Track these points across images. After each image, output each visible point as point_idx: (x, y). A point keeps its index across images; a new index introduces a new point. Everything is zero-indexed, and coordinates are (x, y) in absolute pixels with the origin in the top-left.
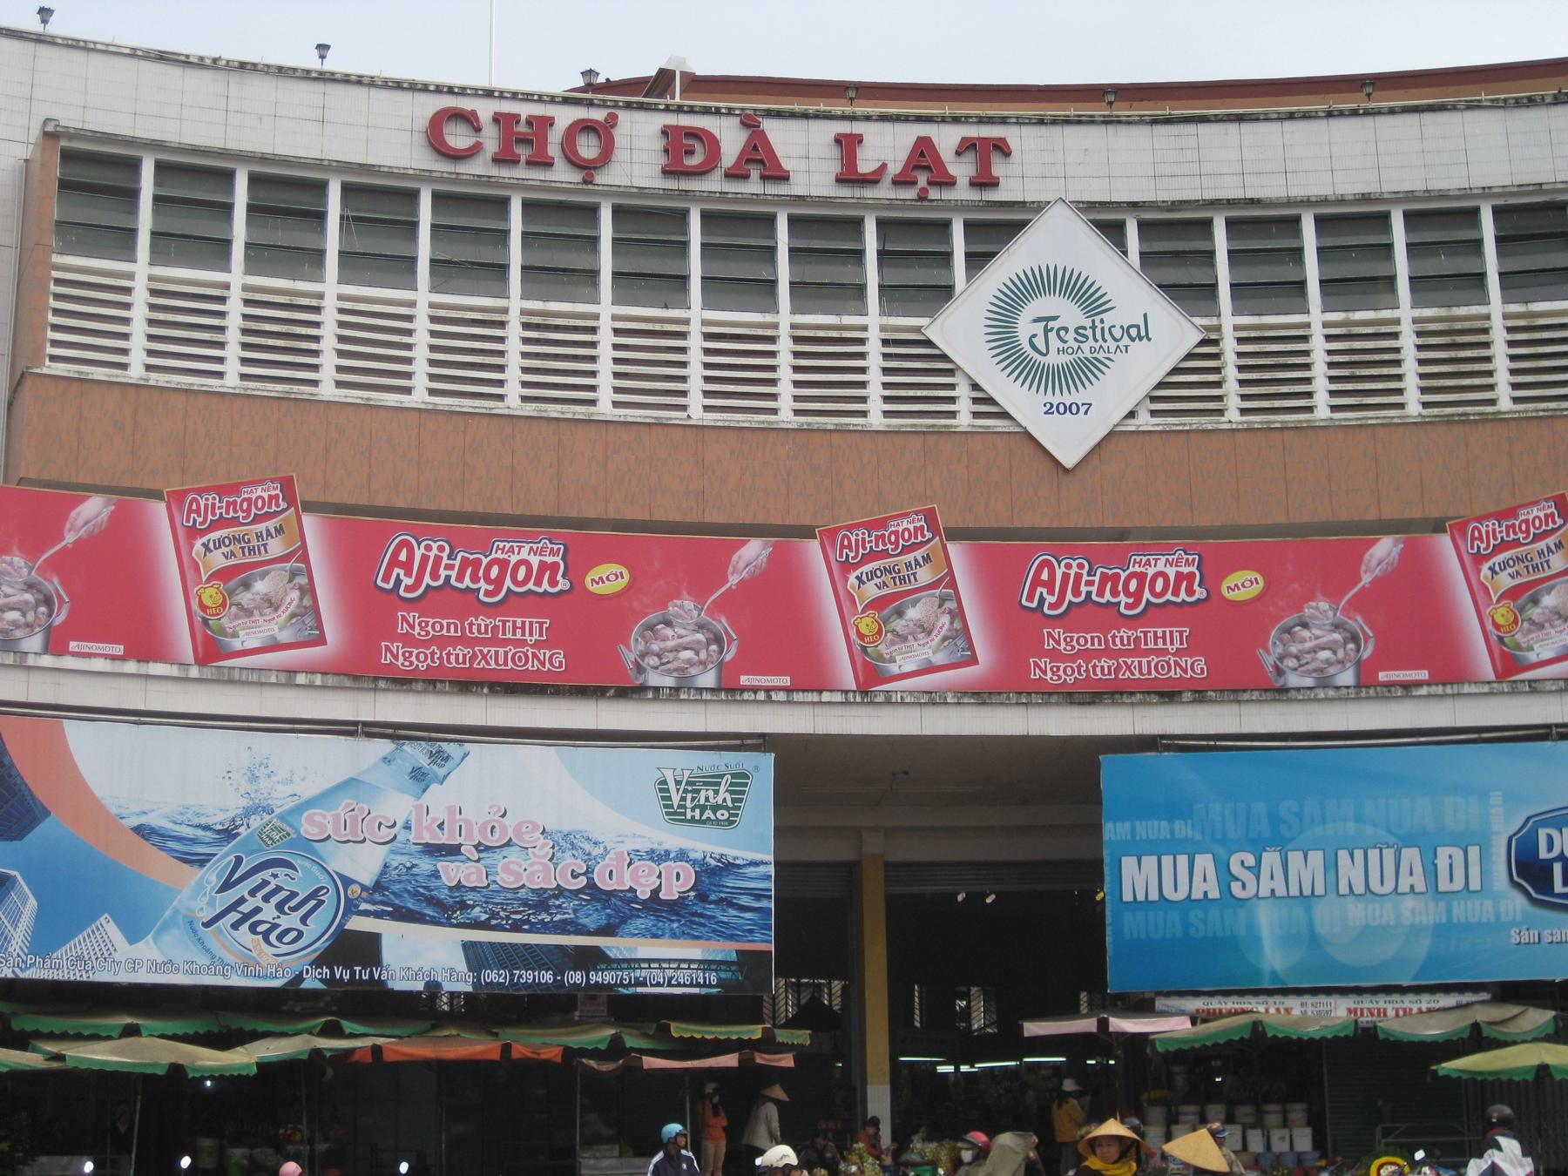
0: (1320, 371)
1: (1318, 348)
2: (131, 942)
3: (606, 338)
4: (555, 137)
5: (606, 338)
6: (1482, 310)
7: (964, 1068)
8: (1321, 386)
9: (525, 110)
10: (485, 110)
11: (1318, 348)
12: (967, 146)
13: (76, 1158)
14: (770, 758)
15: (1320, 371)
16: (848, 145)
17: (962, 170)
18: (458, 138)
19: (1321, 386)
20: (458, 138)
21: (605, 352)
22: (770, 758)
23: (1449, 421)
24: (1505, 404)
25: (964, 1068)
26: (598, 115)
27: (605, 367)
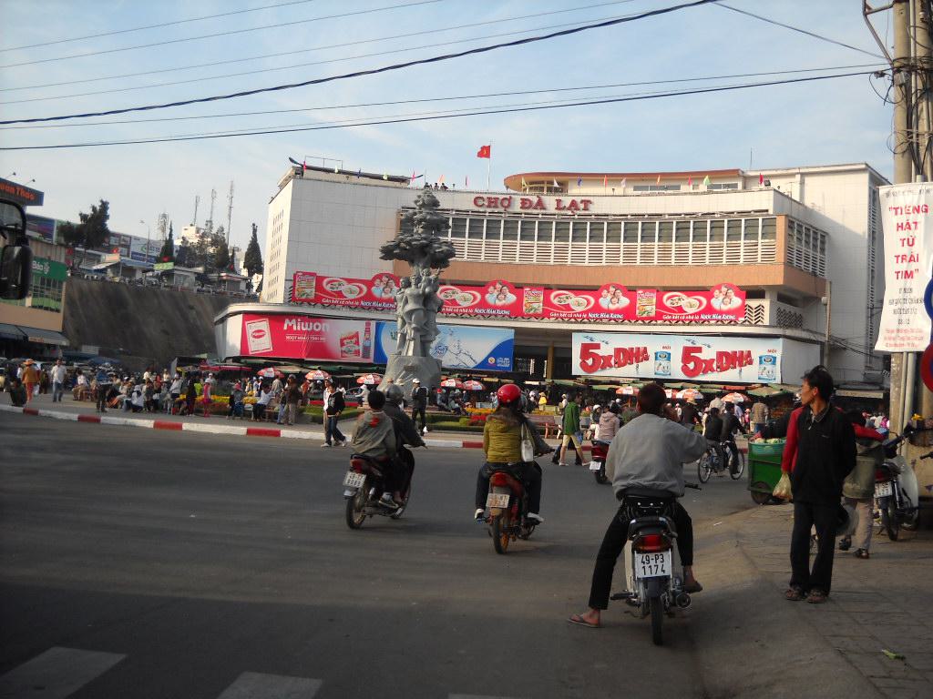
0: (639, 255)
1: (639, 250)
2: (615, 349)
3: (501, 247)
4: (499, 202)
5: (501, 247)
6: (670, 243)
7: (428, 398)
8: (638, 258)
9: (493, 196)
10: (485, 196)
11: (639, 250)
12: (582, 202)
13: (227, 349)
14: (573, 374)
15: (639, 255)
16: (559, 201)
17: (582, 206)
18: (480, 202)
19: (638, 258)
20: (480, 202)
21: (501, 249)
22: (573, 374)
23: (471, 262)
24: (673, 264)
25: (428, 398)
26: (508, 197)
27: (500, 252)
